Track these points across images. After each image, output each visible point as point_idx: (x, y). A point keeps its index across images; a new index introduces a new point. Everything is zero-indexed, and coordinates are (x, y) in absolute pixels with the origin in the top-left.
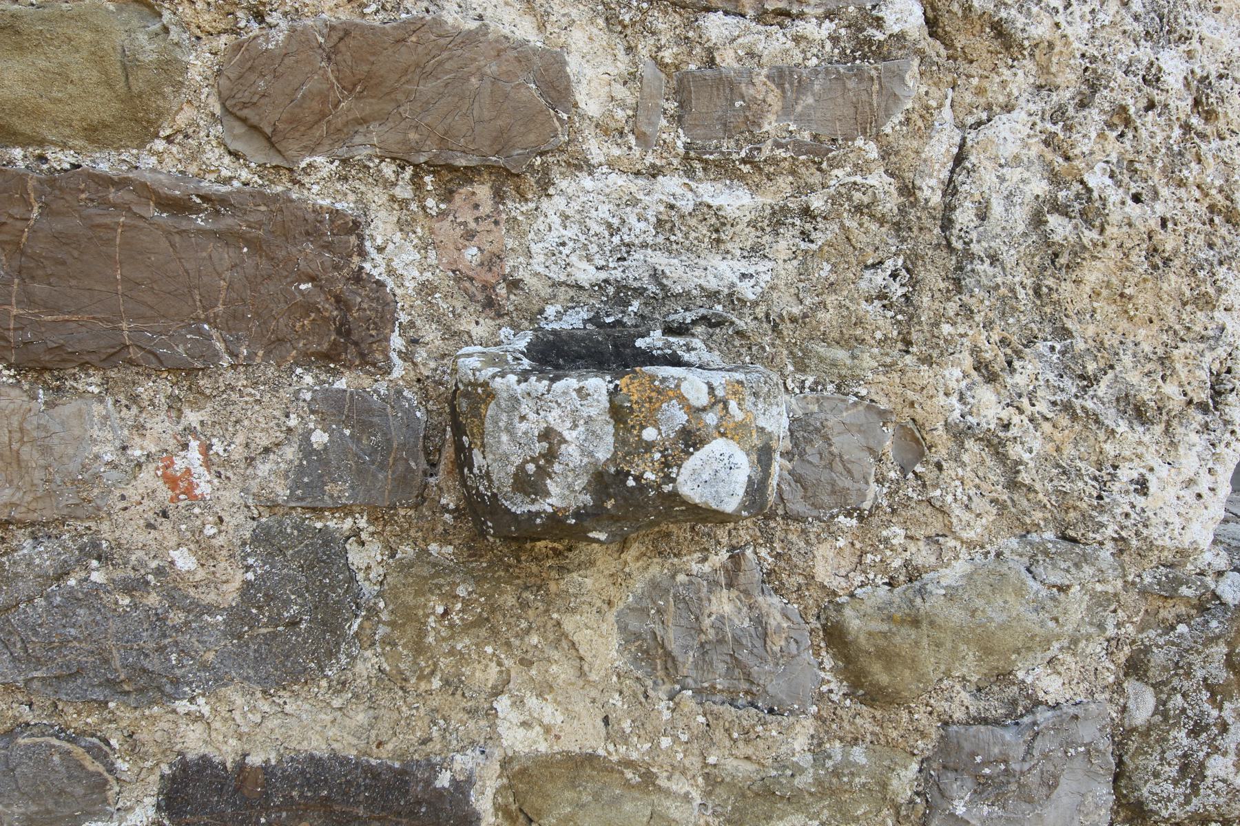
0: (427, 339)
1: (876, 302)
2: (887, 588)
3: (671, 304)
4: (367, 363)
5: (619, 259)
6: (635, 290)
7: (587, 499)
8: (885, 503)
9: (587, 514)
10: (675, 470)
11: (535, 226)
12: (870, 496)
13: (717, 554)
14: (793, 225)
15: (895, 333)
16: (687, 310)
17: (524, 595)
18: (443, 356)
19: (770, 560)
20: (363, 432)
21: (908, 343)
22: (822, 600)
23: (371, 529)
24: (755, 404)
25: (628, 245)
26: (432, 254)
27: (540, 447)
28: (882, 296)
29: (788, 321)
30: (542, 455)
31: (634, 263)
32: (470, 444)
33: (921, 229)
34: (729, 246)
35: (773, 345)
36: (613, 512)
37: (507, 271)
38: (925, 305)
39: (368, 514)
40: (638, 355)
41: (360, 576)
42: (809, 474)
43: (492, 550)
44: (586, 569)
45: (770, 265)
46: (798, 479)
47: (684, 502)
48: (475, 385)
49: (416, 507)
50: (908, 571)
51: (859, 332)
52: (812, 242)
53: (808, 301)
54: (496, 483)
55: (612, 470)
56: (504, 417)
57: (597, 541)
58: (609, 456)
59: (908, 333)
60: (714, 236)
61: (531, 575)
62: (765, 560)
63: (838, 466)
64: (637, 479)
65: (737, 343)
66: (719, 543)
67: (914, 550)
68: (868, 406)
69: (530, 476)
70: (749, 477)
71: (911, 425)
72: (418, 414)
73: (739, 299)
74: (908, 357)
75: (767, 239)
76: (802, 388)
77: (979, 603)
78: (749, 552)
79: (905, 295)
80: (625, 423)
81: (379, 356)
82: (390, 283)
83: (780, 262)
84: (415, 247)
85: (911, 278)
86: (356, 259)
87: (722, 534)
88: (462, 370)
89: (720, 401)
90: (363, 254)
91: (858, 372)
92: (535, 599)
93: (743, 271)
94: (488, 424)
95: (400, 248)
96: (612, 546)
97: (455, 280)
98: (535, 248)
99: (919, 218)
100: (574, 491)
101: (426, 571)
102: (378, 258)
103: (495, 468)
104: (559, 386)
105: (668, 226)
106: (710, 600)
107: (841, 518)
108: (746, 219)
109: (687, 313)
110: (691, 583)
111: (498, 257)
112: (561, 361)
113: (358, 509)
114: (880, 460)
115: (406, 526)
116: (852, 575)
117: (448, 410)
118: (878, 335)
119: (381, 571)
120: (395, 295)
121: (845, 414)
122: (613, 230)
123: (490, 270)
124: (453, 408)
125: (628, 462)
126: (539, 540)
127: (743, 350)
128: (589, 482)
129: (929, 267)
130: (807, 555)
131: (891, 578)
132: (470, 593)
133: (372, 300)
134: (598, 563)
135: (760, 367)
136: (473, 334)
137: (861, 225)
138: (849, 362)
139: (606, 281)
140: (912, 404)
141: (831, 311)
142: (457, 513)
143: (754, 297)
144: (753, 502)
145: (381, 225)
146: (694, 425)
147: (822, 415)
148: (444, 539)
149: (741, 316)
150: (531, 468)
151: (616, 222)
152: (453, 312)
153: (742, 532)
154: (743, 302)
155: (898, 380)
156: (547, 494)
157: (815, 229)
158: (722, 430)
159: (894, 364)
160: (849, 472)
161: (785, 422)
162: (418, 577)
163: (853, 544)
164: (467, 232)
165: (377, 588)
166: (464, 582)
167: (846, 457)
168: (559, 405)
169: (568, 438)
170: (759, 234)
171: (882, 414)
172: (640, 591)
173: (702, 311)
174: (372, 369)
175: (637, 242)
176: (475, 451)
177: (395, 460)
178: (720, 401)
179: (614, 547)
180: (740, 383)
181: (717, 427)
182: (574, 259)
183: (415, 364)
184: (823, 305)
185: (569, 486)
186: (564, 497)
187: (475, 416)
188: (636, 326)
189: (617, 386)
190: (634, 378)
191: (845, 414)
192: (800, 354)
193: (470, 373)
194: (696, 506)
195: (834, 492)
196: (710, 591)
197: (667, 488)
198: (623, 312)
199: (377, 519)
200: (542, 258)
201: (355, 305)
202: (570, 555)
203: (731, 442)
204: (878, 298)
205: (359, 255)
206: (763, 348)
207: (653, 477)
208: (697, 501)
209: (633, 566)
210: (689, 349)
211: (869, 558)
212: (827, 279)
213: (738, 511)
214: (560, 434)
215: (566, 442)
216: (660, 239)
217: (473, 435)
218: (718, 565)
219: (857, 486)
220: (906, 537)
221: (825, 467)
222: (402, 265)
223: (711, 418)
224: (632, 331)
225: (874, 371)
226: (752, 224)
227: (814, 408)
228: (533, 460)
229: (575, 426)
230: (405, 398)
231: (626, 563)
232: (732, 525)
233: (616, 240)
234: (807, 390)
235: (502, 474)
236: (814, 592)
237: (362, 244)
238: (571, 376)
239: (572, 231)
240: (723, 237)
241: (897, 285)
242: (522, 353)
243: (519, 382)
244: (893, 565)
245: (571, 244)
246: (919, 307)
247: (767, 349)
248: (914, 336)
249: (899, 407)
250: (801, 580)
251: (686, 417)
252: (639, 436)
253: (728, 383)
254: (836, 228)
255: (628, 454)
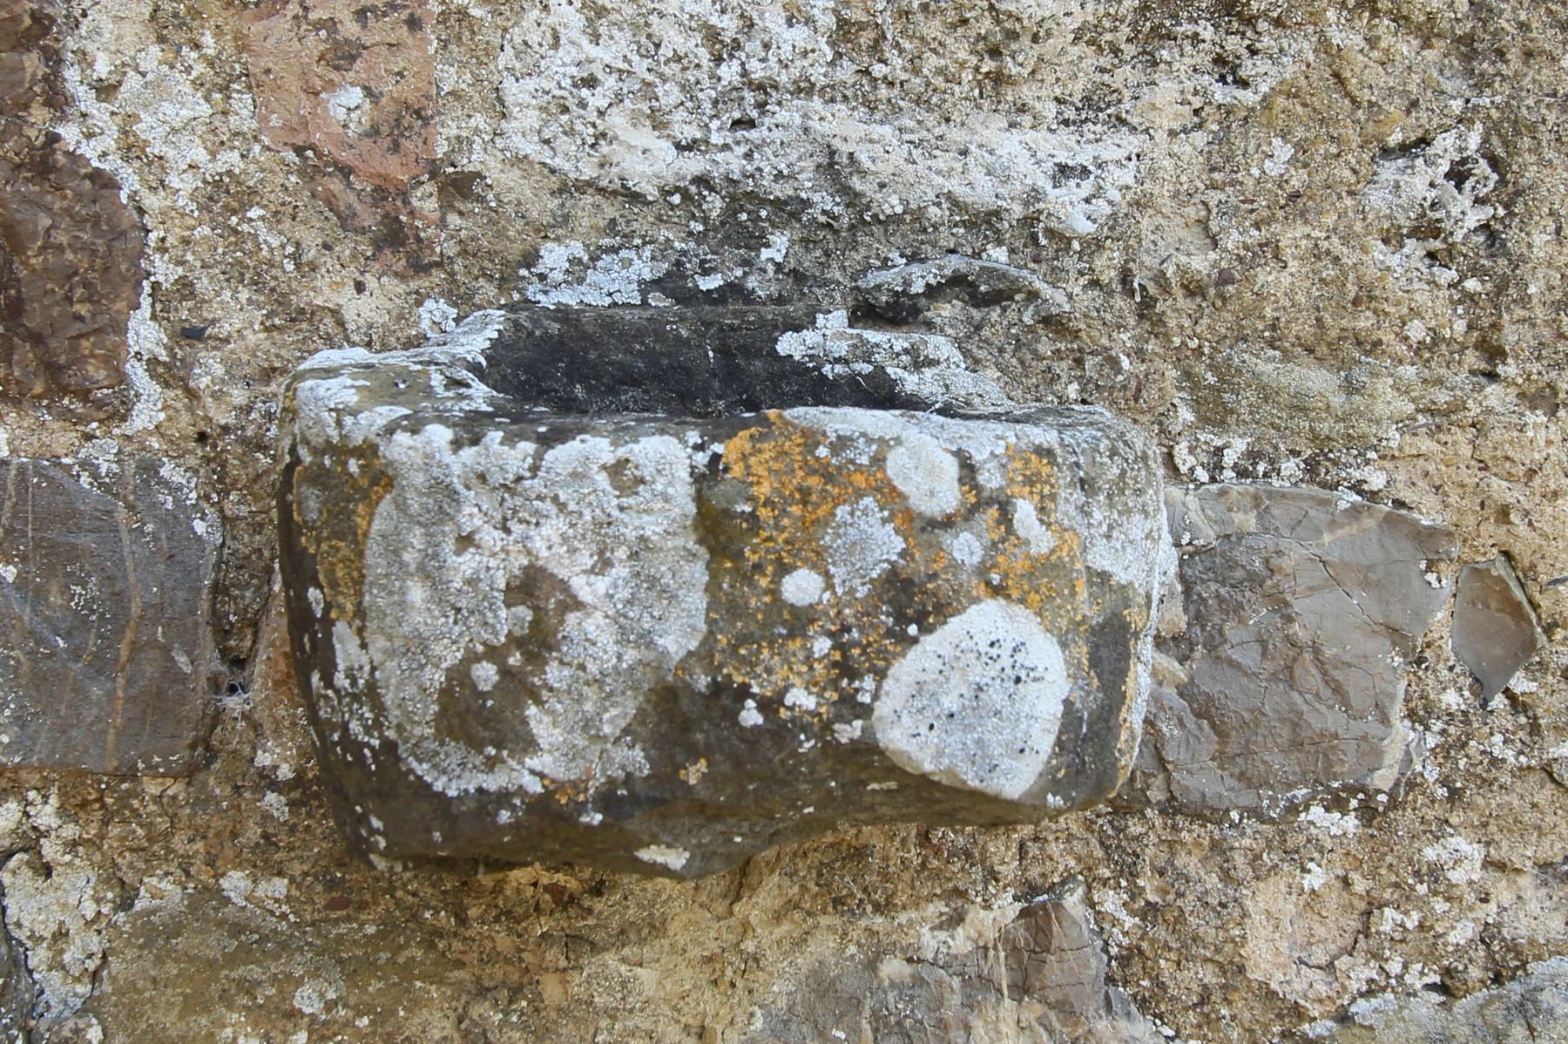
0: (225, 329)
1: (1410, 243)
2: (1436, 998)
3: (872, 245)
4: (65, 390)
5: (737, 124)
6: (778, 204)
7: (635, 758)
8: (1431, 774)
9: (634, 800)
10: (869, 683)
11: (516, 34)
12: (1393, 754)
13: (987, 906)
14: (1195, 39)
15: (1460, 326)
16: (914, 258)
17: (476, 1011)
18: (268, 374)
19: (1129, 922)
20: (50, 572)
21: (1494, 353)
22: (1266, 1029)
23: (71, 831)
24: (1085, 511)
25: (760, 87)
26: (242, 103)
27: (508, 620)
28: (1427, 229)
29: (1179, 292)
30: (515, 641)
31: (778, 135)
32: (328, 607)
33: (1528, 54)
34: (1027, 93)
35: (1139, 354)
36: (704, 794)
37: (441, 150)
38: (1538, 253)
39: (62, 794)
40: (783, 375)
41: (38, 957)
42: (1234, 695)
43: (391, 890)
44: (642, 942)
45: (1133, 143)
46: (1205, 709)
47: (892, 769)
48: (341, 451)
49: (189, 773)
50: (1490, 955)
51: (1365, 321)
52: (1244, 84)
53: (1232, 241)
54: (394, 715)
55: (702, 682)
56: (416, 538)
57: (664, 871)
58: (693, 645)
59: (1495, 326)
60: (988, 65)
61: (493, 957)
62: (1115, 922)
63: (1310, 676)
64: (769, 706)
65: (1045, 348)
66: (993, 876)
67: (1507, 898)
68: (1388, 519)
69: (484, 695)
70: (1067, 703)
71: (1500, 569)
72: (200, 527)
73: (1050, 233)
74: (1492, 389)
75: (1126, 75)
76: (1216, 468)
77: (1357, 474)
78: (1073, 901)
79: (1485, 227)
80: (738, 556)
81: (99, 374)
82: (130, 179)
83: (1161, 136)
84: (198, 84)
85: (1502, 181)
86: (39, 114)
87: (1001, 851)
88: (308, 412)
89: (990, 502)
90: (58, 101)
91: (1363, 427)
92: (505, 1022)
93: (1063, 157)
94: (375, 557)
95: (157, 86)
96: (710, 881)
97: (301, 173)
98: (514, 91)
99: (1524, 27)
100: (599, 738)
101: (213, 945)
102: (99, 112)
103: (391, 671)
104: (563, 455)
105: (866, 38)
106: (968, 1029)
107: (1316, 812)
108: (1073, 24)
109: (916, 269)
110: (918, 981)
111: (418, 113)
112: (579, 390)
113: (35, 779)
114: (1420, 661)
115: (162, 823)
116: (1343, 963)
117: (274, 513)
118: (1416, 330)
119: (95, 944)
120: (141, 211)
121: (1327, 538)
122: (721, 48)
123: (396, 147)
124: (286, 510)
125: (744, 660)
126: (511, 866)
127: (1062, 367)
128: (641, 714)
129: (1549, 154)
130: (1227, 910)
131: (1448, 972)
132: (330, 1006)
133: (80, 222)
134: (673, 927)
135: (1102, 412)
136: (349, 315)
137: (1372, 42)
138: (1338, 400)
139: (702, 181)
140: (1503, 514)
141: (1293, 266)
142: (299, 790)
143: (1086, 228)
144: (1078, 771)
145: (108, 26)
146: (920, 565)
147: (1268, 541)
148: (264, 860)
149: (1056, 277)
150: (486, 674)
151: (729, 25)
152: (295, 258)
153: (1055, 849)
154: (1061, 239)
155: (1466, 451)
156: (529, 745)
157: (1253, 52)
158: (996, 578)
159: (1458, 406)
160: (1338, 690)
161: (1167, 558)
162: (192, 960)
163: (1346, 882)
164: (337, 46)
165: (83, 989)
166: (315, 974)
167: (1329, 652)
168: (562, 507)
169: (585, 595)
170: (1105, 61)
171: (1429, 542)
172: (782, 1003)
173: (955, 263)
174: (78, 407)
175: (783, 78)
176: (341, 628)
177: (135, 648)
178: (990, 502)
179: (715, 884)
180: (1045, 452)
181: (982, 571)
182: (617, 121)
183: (192, 394)
184: (1272, 251)
185: (587, 724)
186: (573, 754)
187: (340, 535)
188: (780, 300)
189: (716, 458)
190: (763, 437)
191: (1327, 538)
192: (1211, 379)
193: (329, 418)
194: (924, 780)
195: (1296, 744)
196: (969, 1005)
197: (849, 732)
198: (746, 263)
199: (84, 805)
200: (532, 119)
201: (33, 236)
202: (599, 905)
203: (1019, 609)
204: (1415, 233)
205: (48, 103)
206: (1114, 363)
207: (810, 702)
208: (928, 767)
209: (765, 937)
210: (919, 362)
211: (1388, 919)
212: (1281, 182)
213: (1038, 793)
214: (564, 586)
215: (578, 605)
216: (846, 72)
217: (334, 584)
218: (991, 934)
219: (1358, 728)
220: (1488, 863)
221: (1274, 678)
222: (162, 130)
223: (966, 547)
224: (769, 312)
225: (1406, 425)
226: (1087, 35)
227: (1248, 521)
228: (493, 653)
229: (603, 564)
230: (166, 483)
231: (746, 926)
232: (1027, 830)
233: (729, 72)
234: (1229, 474)
235: (410, 690)
236: (1243, 1008)
237: (56, 73)
238: (595, 432)
239: (613, 49)
240: (1012, 68)
241: (1465, 201)
242: (474, 368)
243: (457, 445)
244: (1452, 938)
245: (610, 82)
246: (1523, 259)
247: (1125, 363)
248: (1510, 335)
249: (1471, 520)
250: (1209, 976)
251: (899, 544)
252: (775, 592)
253: (1013, 453)
254: (1307, 49)
255: (744, 639)
